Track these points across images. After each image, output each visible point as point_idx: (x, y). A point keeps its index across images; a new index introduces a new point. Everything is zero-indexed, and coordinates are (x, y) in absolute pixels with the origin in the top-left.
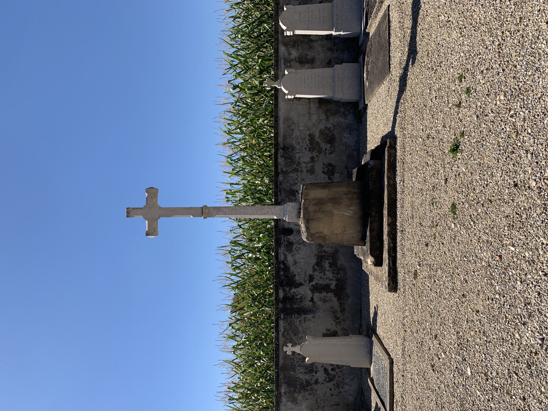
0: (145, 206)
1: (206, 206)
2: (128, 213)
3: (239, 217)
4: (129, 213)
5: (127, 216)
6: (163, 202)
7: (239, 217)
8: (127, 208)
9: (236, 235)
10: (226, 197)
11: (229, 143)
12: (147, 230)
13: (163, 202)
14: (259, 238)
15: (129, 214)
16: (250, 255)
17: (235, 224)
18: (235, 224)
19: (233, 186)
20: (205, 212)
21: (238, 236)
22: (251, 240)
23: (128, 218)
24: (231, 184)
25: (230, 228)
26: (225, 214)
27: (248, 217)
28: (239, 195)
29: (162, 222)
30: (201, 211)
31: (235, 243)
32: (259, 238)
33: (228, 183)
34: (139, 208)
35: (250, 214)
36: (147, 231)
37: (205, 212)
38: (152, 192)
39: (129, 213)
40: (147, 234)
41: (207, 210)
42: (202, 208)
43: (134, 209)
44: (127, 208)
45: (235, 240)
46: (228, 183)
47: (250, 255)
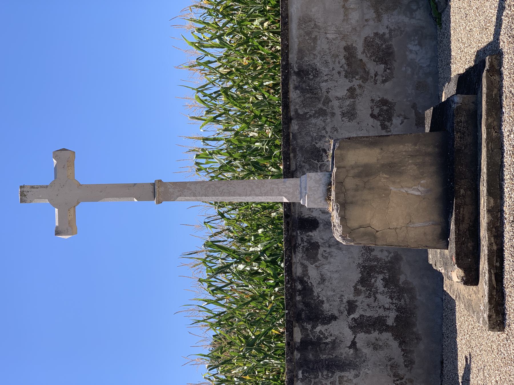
0: (53, 183)
1: (160, 181)
2: (22, 194)
5: (22, 201)
6: (85, 174)
10: (197, 164)
11: (200, 64)
12: (57, 224)
13: (85, 174)
14: (256, 236)
16: (241, 267)
18: (214, 211)
20: (158, 191)
21: (219, 233)
23: (23, 204)
24: (205, 139)
26: (194, 195)
28: (219, 160)
30: (152, 190)
31: (212, 245)
32: (256, 236)
33: (198, 139)
35: (240, 195)
37: (158, 191)
38: (65, 157)
39: (24, 195)
41: (162, 189)
42: (154, 185)
43: (32, 187)
45: (213, 239)
46: (198, 139)
47: (241, 267)
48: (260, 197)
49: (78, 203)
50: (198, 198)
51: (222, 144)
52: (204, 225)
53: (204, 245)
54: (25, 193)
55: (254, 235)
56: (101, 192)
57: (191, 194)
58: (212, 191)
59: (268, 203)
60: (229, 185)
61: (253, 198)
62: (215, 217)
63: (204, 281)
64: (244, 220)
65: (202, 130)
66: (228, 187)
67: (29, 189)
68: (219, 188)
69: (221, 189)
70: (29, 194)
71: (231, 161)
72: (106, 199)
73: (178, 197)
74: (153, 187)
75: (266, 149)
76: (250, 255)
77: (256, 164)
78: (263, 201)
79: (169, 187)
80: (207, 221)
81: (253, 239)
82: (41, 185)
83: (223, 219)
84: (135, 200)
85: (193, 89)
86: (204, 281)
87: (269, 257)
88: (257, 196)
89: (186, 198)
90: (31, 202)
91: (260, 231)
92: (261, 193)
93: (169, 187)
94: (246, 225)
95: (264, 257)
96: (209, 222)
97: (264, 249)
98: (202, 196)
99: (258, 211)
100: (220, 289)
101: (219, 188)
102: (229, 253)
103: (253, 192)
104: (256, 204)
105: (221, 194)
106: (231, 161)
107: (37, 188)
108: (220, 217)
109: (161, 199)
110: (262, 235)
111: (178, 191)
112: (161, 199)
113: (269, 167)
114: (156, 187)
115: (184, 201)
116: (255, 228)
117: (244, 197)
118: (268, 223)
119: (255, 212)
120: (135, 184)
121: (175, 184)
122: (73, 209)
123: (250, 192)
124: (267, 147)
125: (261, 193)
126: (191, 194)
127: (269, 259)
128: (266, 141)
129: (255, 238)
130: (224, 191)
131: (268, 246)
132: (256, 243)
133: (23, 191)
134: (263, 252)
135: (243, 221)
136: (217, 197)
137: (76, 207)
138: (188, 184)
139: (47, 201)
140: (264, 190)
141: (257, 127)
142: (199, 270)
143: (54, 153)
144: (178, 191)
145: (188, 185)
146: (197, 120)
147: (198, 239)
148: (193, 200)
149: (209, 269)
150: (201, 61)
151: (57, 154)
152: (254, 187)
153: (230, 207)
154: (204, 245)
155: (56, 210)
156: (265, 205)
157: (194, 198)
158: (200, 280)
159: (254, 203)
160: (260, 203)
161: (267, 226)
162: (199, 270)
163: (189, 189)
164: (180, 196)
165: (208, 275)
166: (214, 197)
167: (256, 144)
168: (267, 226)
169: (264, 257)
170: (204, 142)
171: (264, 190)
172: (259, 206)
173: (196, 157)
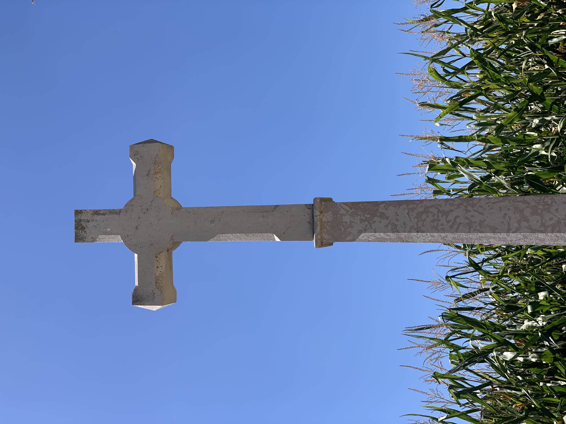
0: (130, 205)
1: (327, 201)
2: (80, 226)
3: (476, 239)
4: (84, 227)
5: (78, 239)
6: (192, 186)
7: (476, 239)
8: (77, 212)
9: (465, 291)
10: (431, 181)
11: (437, 15)
12: (137, 284)
13: (192, 186)
14: (536, 305)
15: (81, 232)
16: (509, 355)
17: (462, 259)
18: (462, 259)
19: (449, 144)
20: (325, 222)
21: (473, 295)
22: (511, 307)
23: (80, 244)
24: (443, 140)
25: (445, 272)
26: (395, 230)
27: (500, 240)
28: (467, 177)
29: (188, 257)
30: (308, 218)
31: (457, 319)
32: (536, 305)
33: (434, 139)
34: (112, 212)
35: (494, 230)
36: (136, 289)
37: (325, 222)
38: (154, 158)
39: (84, 227)
40: (137, 299)
41: (328, 217)
42: (311, 207)
43: (96, 213)
44: (77, 212)
45: (461, 304)
46: (434, 139)
47: (509, 355)
48: (541, 236)
49: (176, 244)
50: (403, 235)
51: (472, 149)
52: (446, 282)
53: (442, 316)
54: (83, 223)
55: (531, 304)
56: (212, 222)
57: (386, 226)
58: (433, 221)
59: (555, 248)
60: (469, 208)
61: (525, 237)
62: (465, 269)
63: (443, 377)
64: (515, 276)
65: (437, 124)
66: (468, 211)
67: (89, 217)
68: (446, 214)
69: (451, 217)
70: (90, 224)
71: (489, 177)
72: (223, 236)
73: (360, 232)
74: (310, 211)
75: (551, 156)
76: (524, 336)
77: (534, 181)
78: (547, 243)
79: (342, 212)
80: (450, 274)
81: (530, 311)
82: (111, 208)
83: (477, 273)
84: (277, 239)
85: (426, 58)
86: (443, 377)
87: (556, 341)
88: (533, 231)
89: (377, 234)
90: (94, 240)
91: (541, 295)
92: (543, 225)
93: (342, 212)
94: (517, 283)
95: (549, 341)
96: (453, 277)
97: (549, 327)
98: (410, 232)
99: (538, 261)
100: (471, 391)
101: (446, 214)
102: (485, 331)
103: (524, 224)
104: (534, 249)
105: (451, 227)
106: (489, 177)
107: (104, 214)
108: (472, 269)
109: (327, 237)
110: (544, 303)
111: (362, 221)
112: (327, 237)
113: (558, 185)
114: (317, 213)
115: (374, 241)
116: (533, 289)
117: (504, 235)
118: (556, 282)
119: (534, 262)
120: (276, 206)
121: (355, 205)
122: (163, 256)
123: (519, 222)
124: (554, 154)
125: (543, 225)
126: (386, 226)
127: (557, 346)
128: (553, 139)
129: (533, 309)
130: (458, 220)
131: (555, 323)
132: (534, 315)
133: (80, 220)
134: (547, 333)
135: (511, 276)
136: (443, 235)
137: (174, 252)
138: (382, 206)
139: (118, 240)
140: (551, 219)
141: (537, 117)
142: (436, 356)
143: (132, 147)
144: (362, 221)
145: (381, 209)
146: (431, 109)
147: (432, 306)
148: (391, 240)
149: (454, 353)
150: (441, 9)
151: (136, 151)
152: (527, 212)
153: (492, 252)
154: (442, 316)
155: (136, 255)
156: (551, 251)
157: (393, 235)
158: (436, 376)
159: (530, 246)
160: (541, 248)
161: (553, 286)
162: (436, 356)
163: (382, 216)
164: (365, 231)
165: (452, 362)
166: (436, 234)
167: (534, 147)
168: (553, 286)
169: (549, 341)
170: (442, 144)
171: (551, 219)
172: (540, 253)
173: (429, 169)
